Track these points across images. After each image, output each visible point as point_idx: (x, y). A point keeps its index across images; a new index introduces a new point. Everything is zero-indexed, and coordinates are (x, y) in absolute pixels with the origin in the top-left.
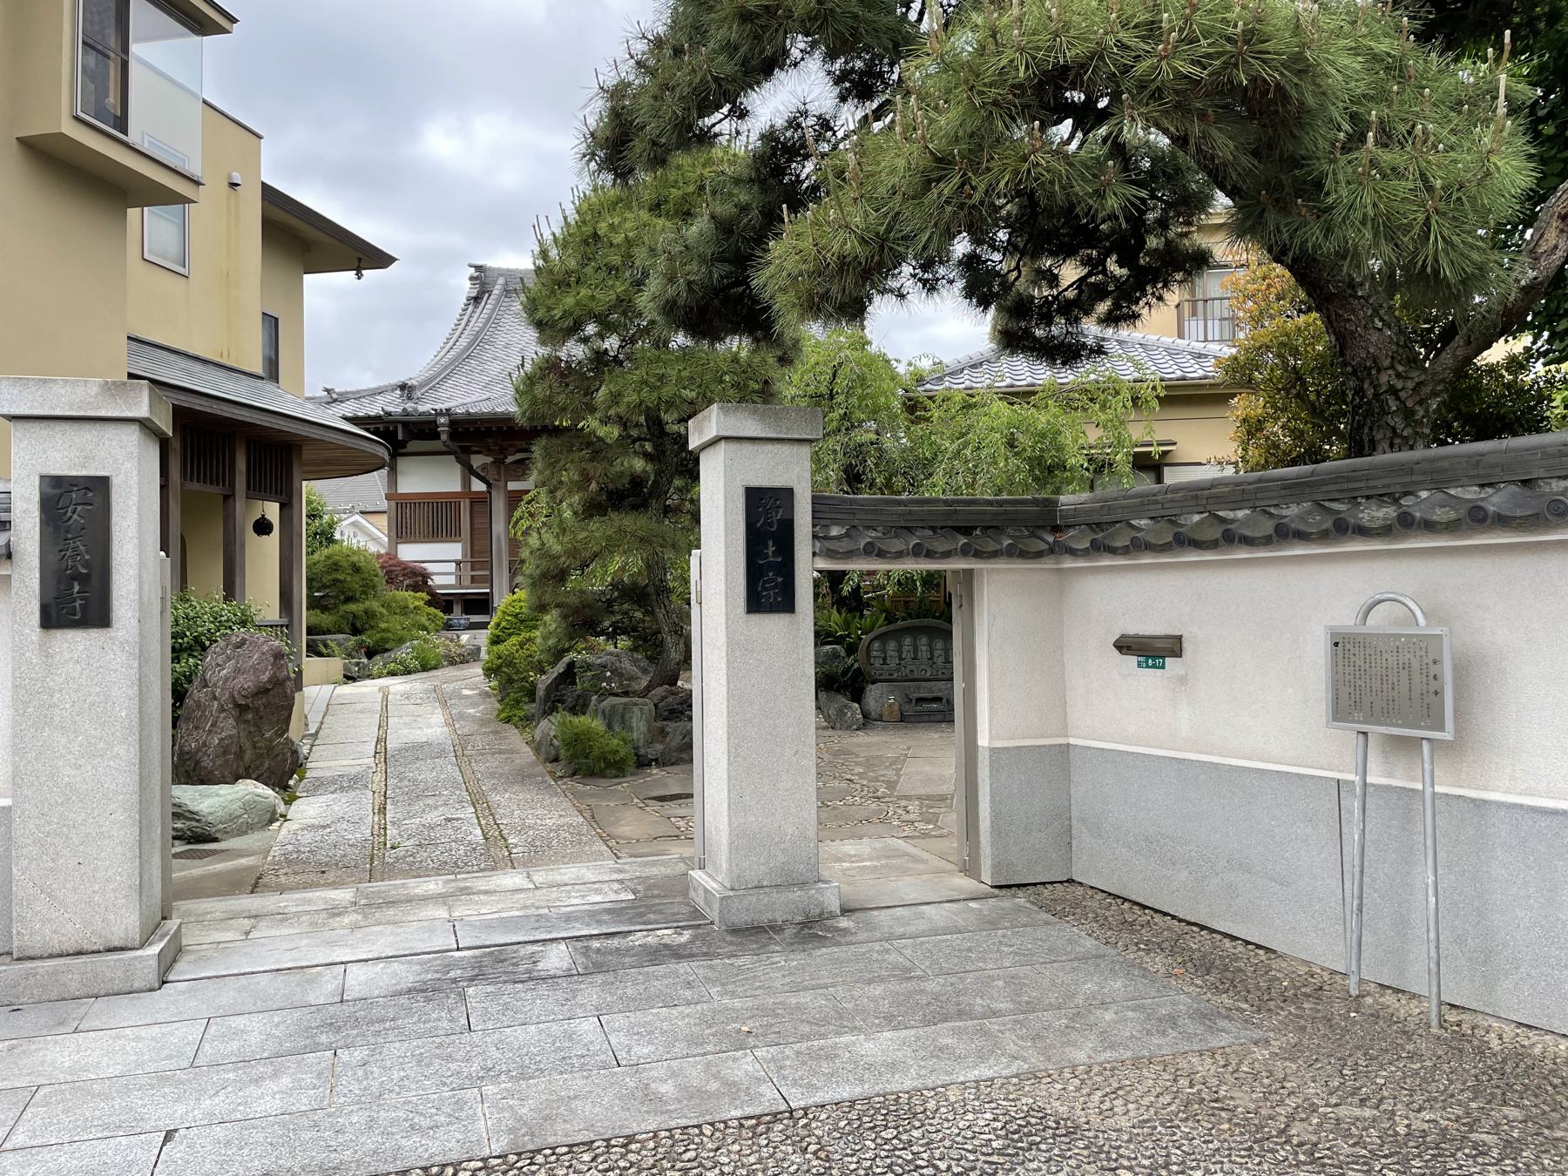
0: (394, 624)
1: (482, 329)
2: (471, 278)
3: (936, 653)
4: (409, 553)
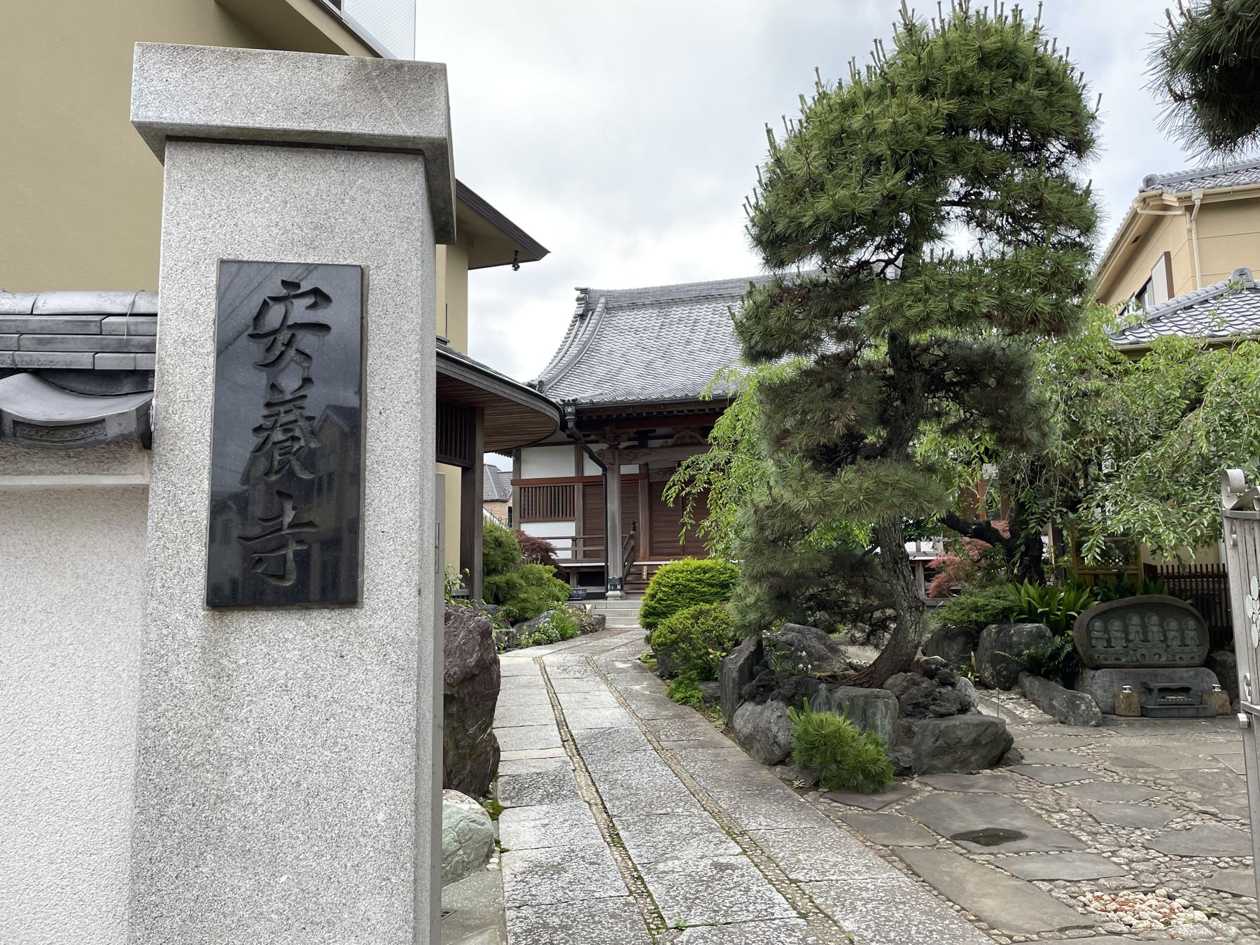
0: (531, 594)
1: (589, 339)
2: (578, 299)
3: (1171, 635)
4: (534, 530)
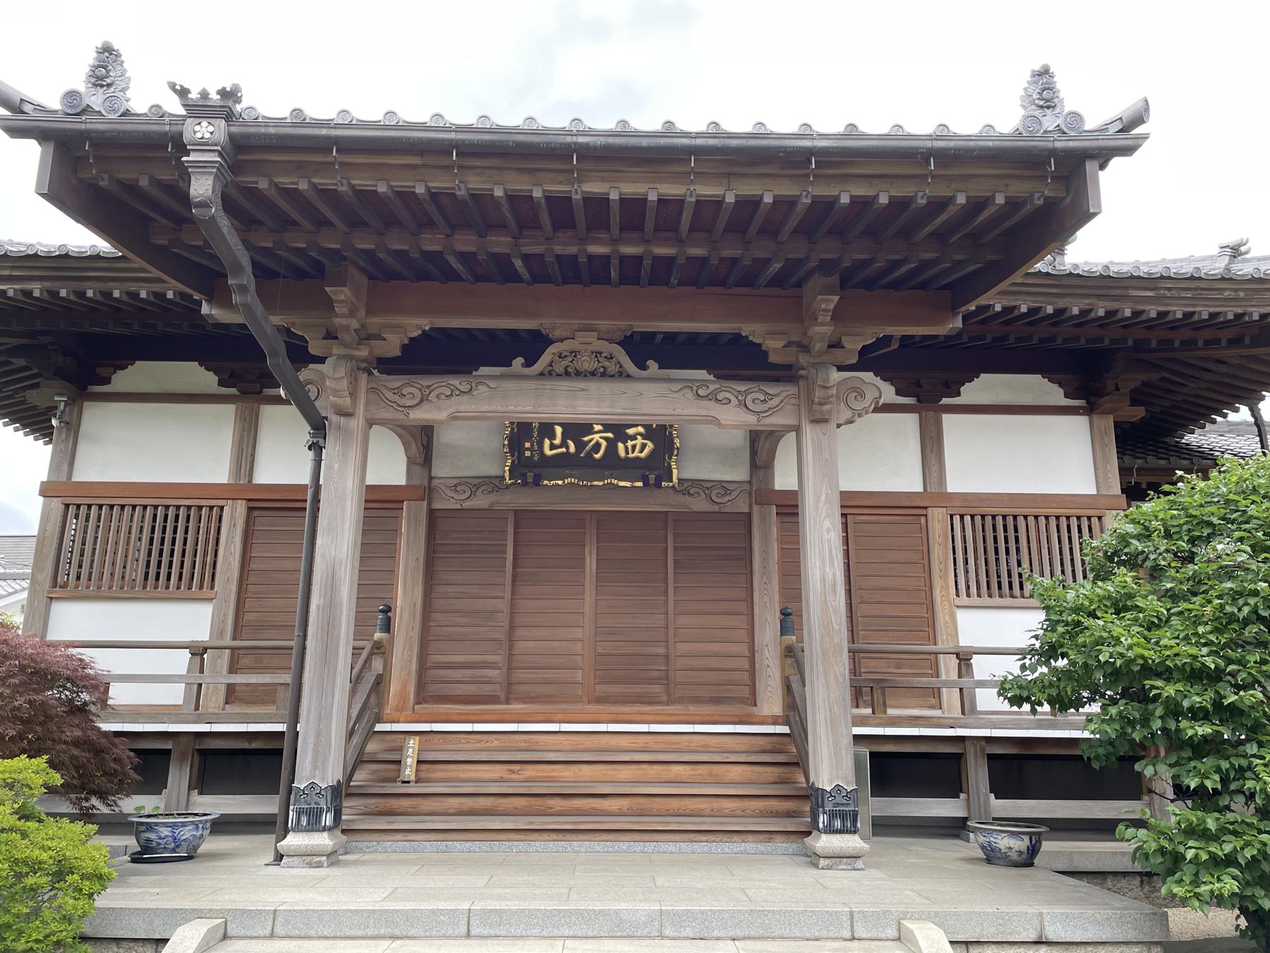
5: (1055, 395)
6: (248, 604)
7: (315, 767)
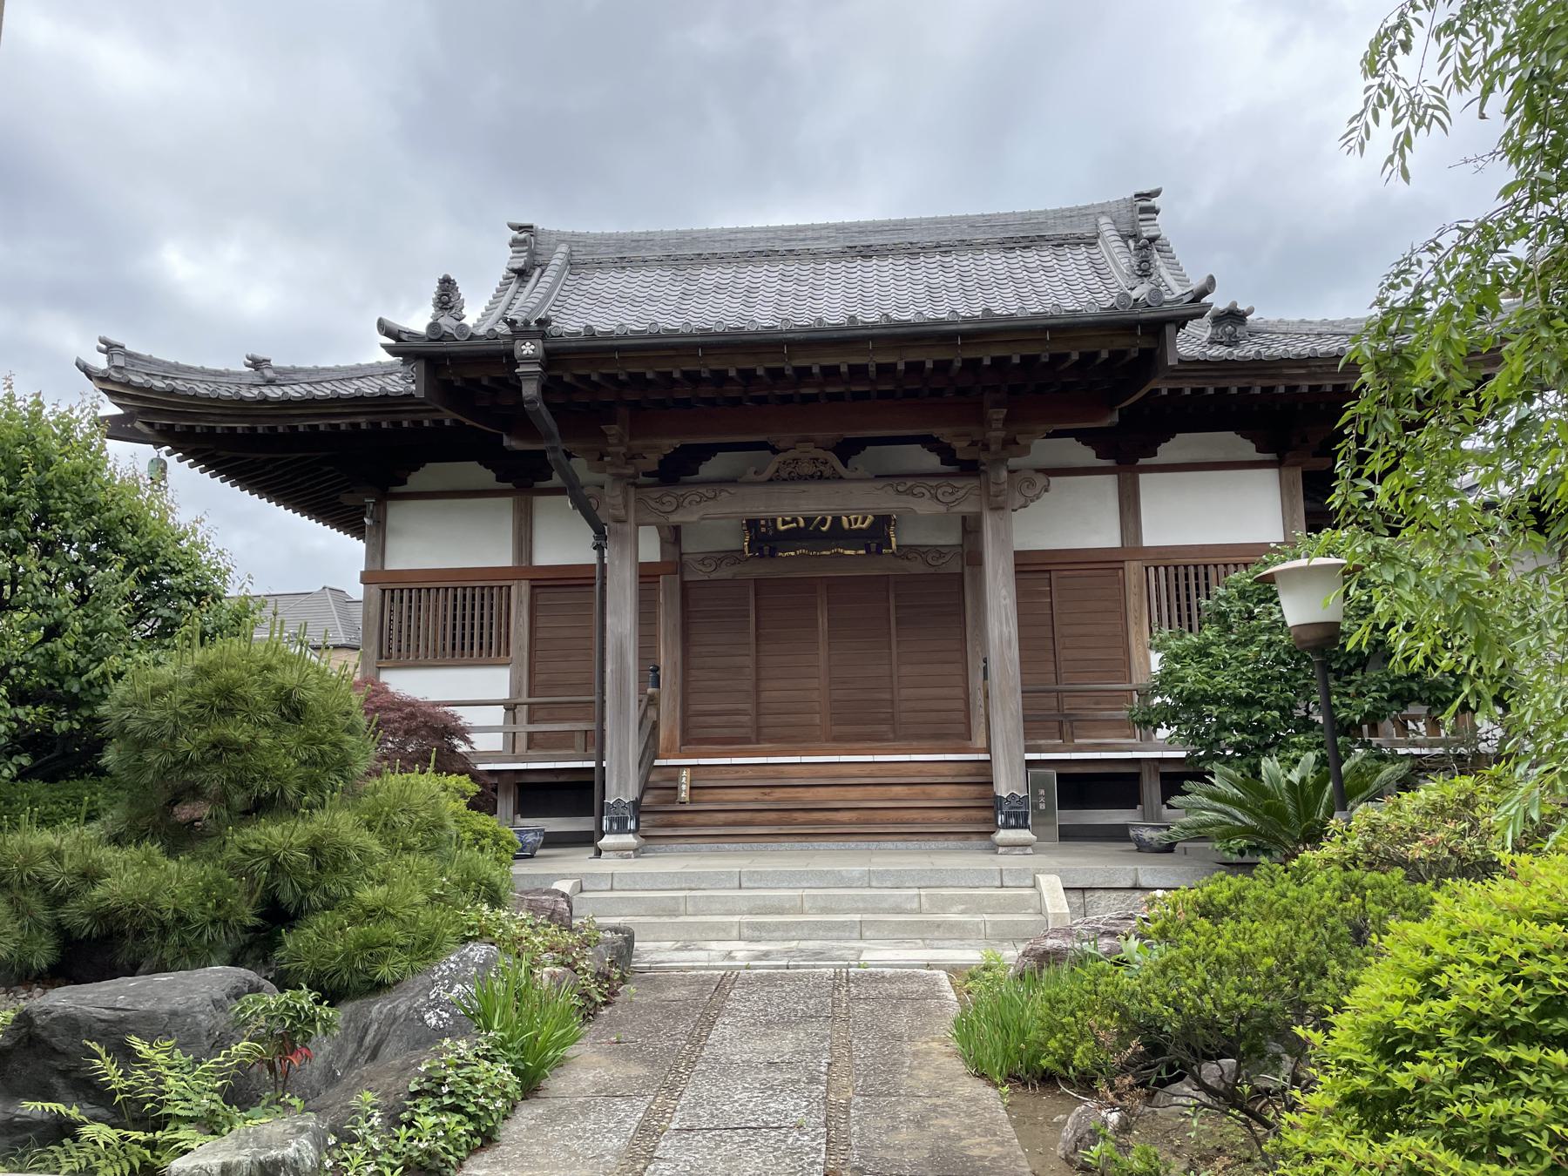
2: (515, 243)
4: (415, 685)
5: (1248, 450)
6: (538, 667)
7: (619, 788)
